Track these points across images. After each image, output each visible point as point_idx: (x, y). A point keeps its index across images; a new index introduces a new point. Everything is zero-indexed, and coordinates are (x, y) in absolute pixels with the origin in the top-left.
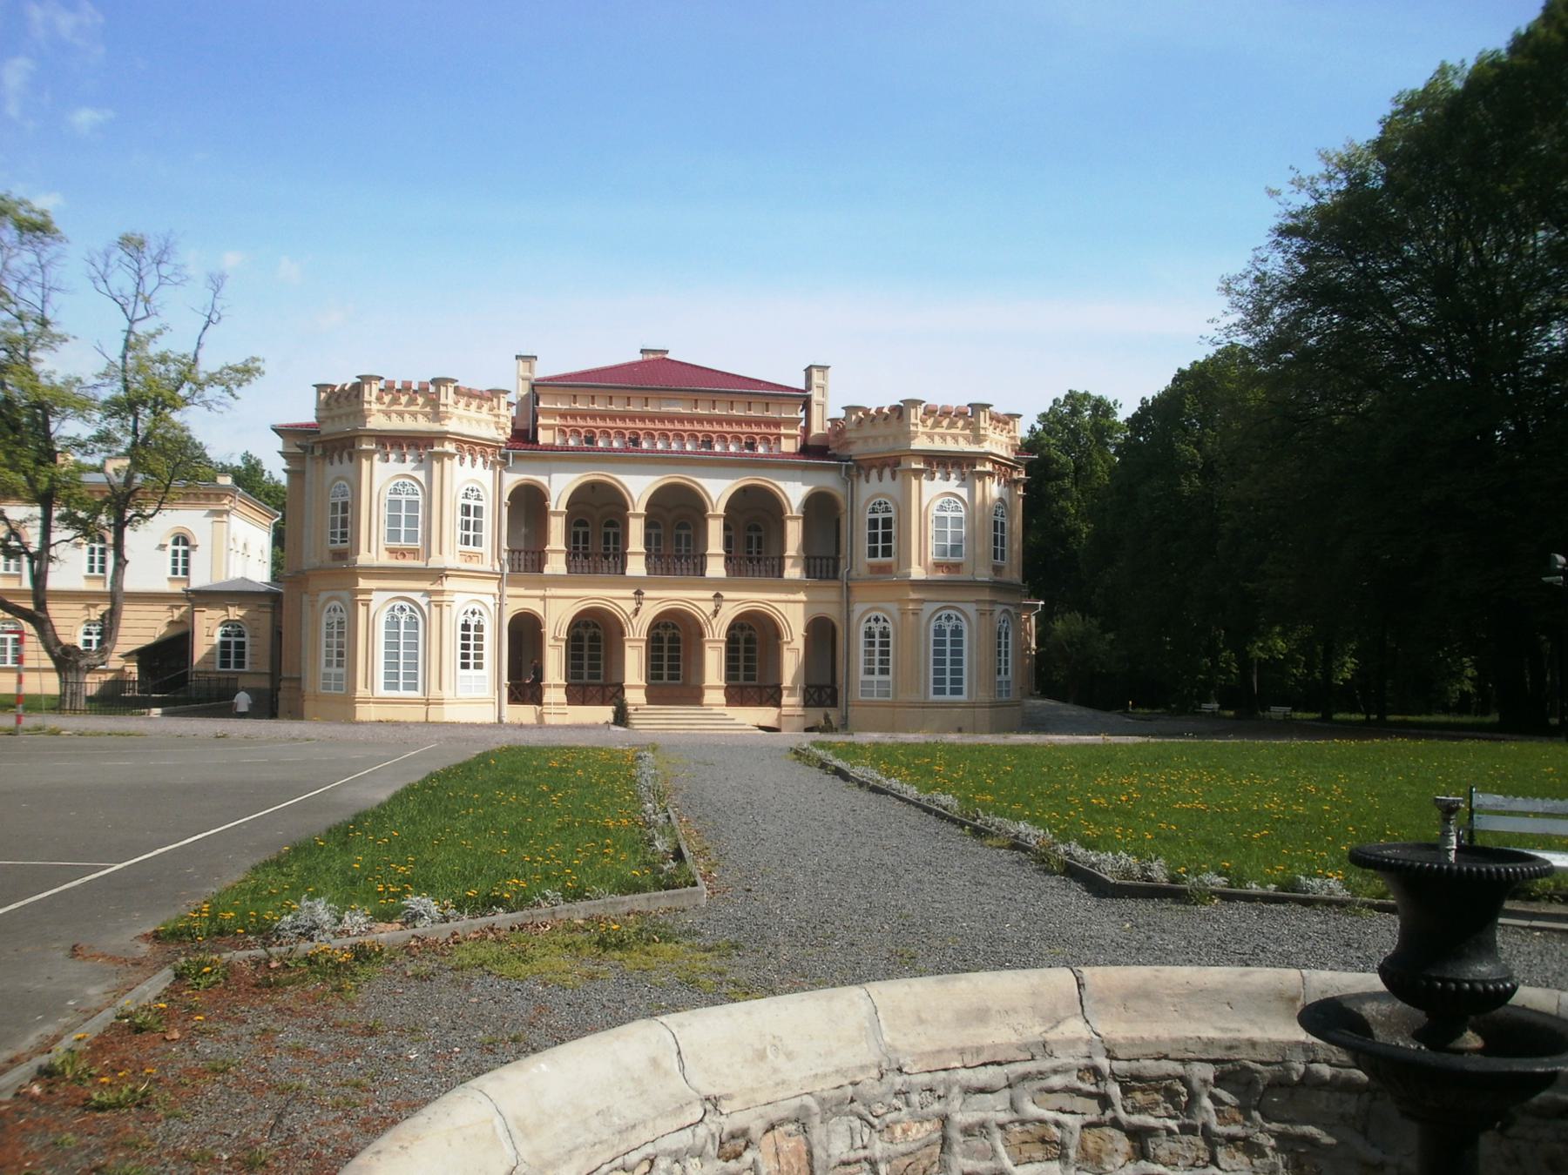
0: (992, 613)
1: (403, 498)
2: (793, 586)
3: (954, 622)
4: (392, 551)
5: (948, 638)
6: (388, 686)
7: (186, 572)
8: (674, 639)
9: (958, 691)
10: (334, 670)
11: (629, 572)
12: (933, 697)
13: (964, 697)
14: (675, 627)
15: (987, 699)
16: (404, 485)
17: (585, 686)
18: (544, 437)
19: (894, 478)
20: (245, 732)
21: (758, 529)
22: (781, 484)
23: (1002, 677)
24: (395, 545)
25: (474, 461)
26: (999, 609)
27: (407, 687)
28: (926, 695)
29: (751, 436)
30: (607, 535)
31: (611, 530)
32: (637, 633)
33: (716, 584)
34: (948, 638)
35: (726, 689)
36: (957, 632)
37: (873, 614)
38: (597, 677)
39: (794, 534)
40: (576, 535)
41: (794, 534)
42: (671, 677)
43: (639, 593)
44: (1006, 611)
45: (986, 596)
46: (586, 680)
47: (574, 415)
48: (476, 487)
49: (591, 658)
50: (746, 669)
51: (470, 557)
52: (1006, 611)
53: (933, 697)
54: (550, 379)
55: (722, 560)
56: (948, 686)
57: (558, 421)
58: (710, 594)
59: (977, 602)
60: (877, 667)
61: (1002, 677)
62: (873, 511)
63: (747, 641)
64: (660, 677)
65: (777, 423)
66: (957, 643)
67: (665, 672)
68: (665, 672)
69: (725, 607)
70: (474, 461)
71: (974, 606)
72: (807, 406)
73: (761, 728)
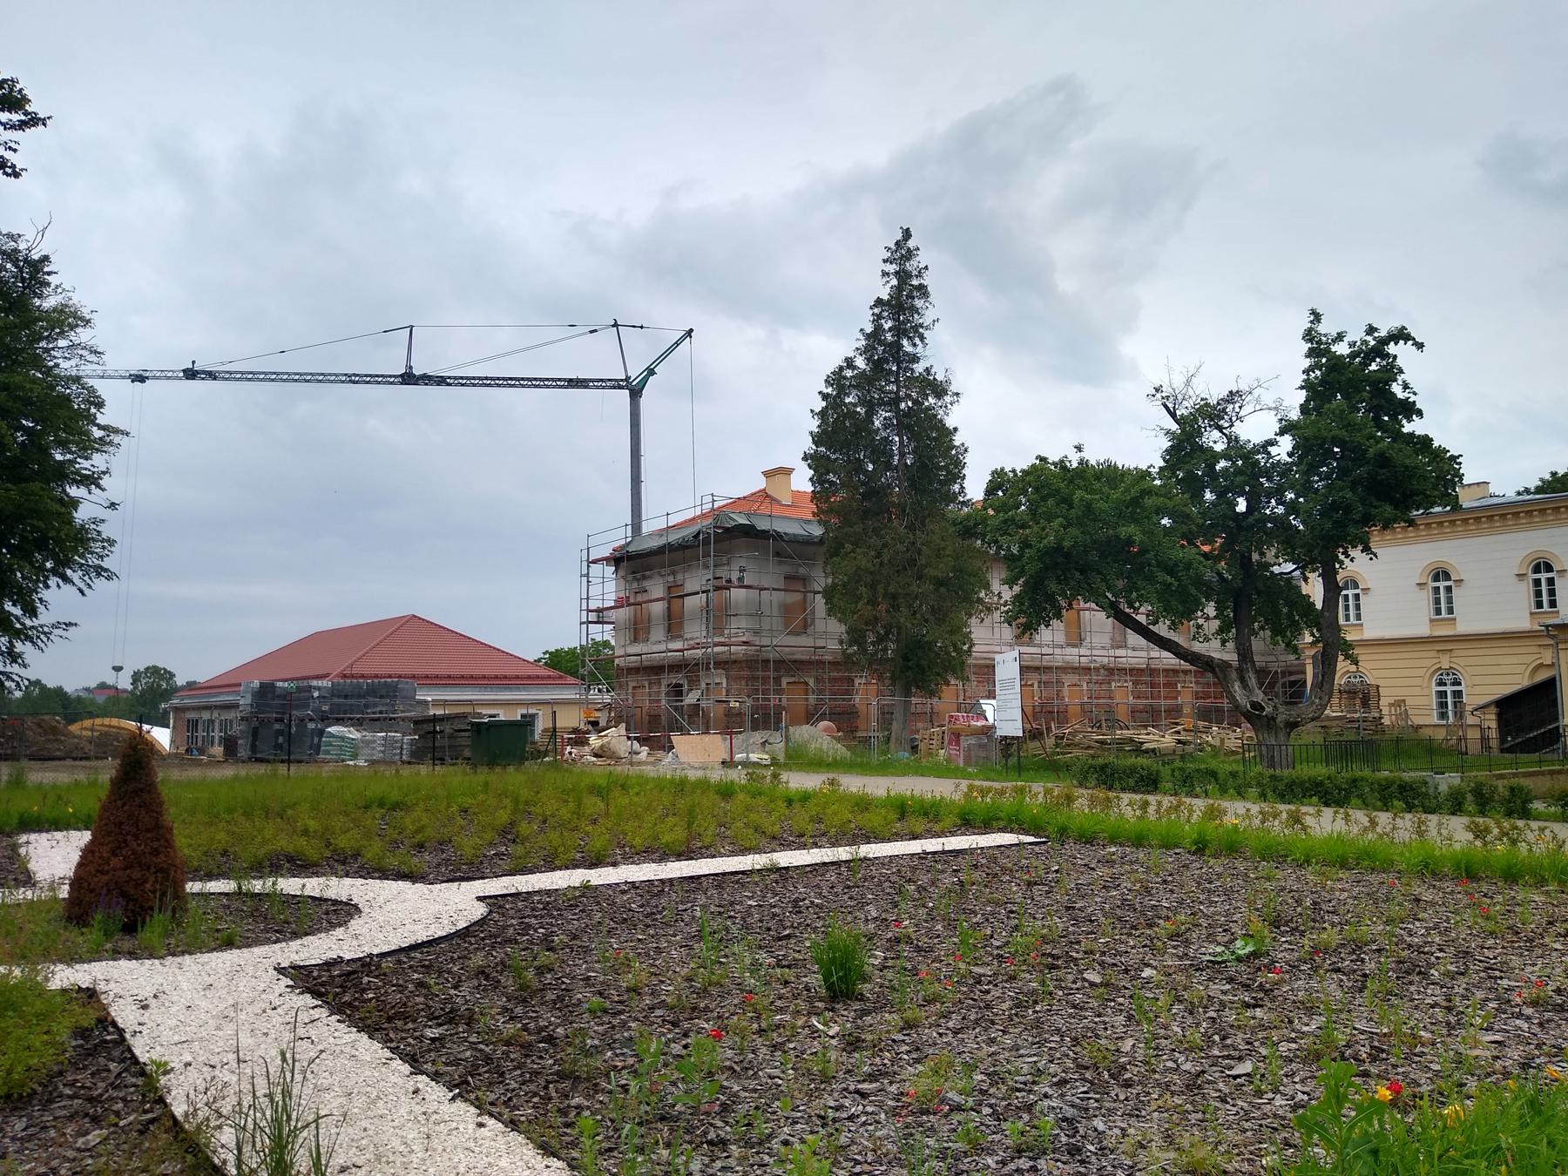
7: (1553, 604)
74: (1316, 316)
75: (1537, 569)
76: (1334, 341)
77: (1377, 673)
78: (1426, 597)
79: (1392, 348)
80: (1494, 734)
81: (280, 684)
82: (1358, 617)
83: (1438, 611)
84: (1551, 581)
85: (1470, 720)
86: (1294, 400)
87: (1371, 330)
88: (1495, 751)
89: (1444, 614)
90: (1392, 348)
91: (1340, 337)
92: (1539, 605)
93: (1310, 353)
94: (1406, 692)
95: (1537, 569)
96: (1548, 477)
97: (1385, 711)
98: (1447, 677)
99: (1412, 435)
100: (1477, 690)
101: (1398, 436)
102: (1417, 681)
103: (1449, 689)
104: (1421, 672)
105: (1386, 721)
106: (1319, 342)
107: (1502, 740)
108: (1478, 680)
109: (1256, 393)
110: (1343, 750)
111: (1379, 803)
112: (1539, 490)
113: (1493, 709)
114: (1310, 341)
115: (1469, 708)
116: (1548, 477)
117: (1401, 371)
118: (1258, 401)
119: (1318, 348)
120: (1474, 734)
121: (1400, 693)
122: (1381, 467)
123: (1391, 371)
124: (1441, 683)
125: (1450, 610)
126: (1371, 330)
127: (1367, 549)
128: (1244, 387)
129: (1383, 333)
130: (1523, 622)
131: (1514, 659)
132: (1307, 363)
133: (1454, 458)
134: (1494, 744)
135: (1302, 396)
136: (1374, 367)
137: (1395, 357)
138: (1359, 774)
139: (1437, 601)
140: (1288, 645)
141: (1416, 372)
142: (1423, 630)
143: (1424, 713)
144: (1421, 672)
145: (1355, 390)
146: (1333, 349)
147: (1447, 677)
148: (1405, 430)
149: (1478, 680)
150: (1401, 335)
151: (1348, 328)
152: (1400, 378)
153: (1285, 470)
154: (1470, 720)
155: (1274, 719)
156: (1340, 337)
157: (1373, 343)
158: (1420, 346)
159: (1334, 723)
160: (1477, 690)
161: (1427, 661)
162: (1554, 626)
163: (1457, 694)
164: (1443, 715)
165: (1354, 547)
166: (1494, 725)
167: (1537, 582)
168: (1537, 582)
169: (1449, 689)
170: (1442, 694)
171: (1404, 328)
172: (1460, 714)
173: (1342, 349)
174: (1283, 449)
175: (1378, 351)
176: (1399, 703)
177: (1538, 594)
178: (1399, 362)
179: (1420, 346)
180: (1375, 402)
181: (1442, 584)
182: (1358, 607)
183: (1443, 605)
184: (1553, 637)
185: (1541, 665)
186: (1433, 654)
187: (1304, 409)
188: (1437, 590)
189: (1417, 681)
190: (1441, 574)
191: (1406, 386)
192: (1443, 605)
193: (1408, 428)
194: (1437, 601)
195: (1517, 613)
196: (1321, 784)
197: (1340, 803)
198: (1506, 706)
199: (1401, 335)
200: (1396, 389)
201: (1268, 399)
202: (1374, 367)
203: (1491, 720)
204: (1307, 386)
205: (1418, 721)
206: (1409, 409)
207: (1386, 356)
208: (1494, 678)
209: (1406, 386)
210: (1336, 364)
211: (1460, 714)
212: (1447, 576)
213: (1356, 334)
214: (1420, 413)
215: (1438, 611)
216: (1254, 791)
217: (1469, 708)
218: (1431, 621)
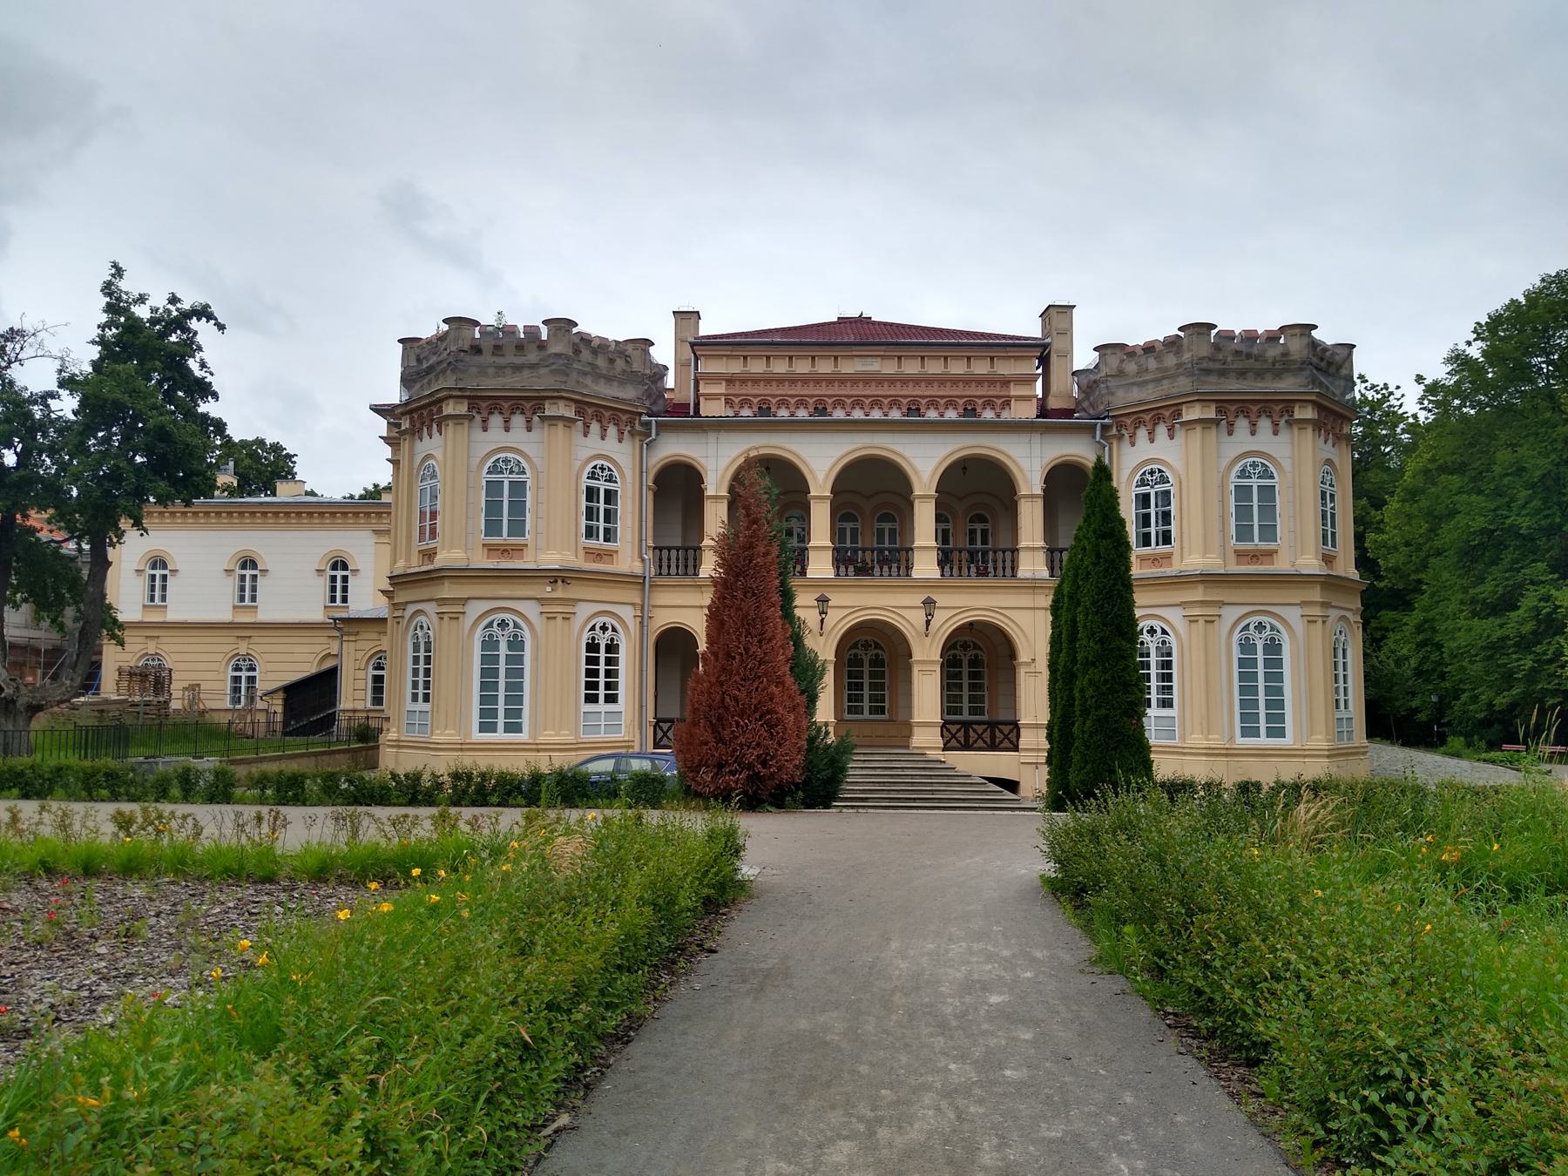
0: (1325, 618)
1: (1255, 482)
2: (1033, 586)
3: (1268, 632)
4: (491, 549)
5: (1260, 656)
6: (484, 728)
7: (345, 599)
8: (877, 662)
9: (517, 728)
10: (421, 706)
11: (915, 574)
12: (1242, 742)
13: (523, 737)
14: (877, 646)
15: (1324, 745)
16: (506, 461)
17: (966, 725)
18: (708, 409)
19: (1172, 437)
20: (1443, 776)
21: (982, 519)
22: (950, 449)
23: (1342, 713)
24: (495, 540)
25: (604, 430)
26: (1334, 614)
27: (1271, 733)
28: (1232, 738)
29: (970, 400)
30: (972, 532)
31: (979, 527)
32: (927, 654)
33: (926, 584)
34: (1260, 656)
35: (945, 726)
36: (1273, 647)
37: (600, 621)
38: (980, 711)
39: (1031, 519)
40: (842, 531)
41: (1031, 519)
42: (873, 711)
43: (823, 600)
44: (1343, 618)
45: (1316, 594)
46: (966, 716)
47: (744, 380)
48: (606, 464)
49: (873, 686)
50: (972, 699)
51: (599, 555)
52: (1343, 618)
53: (479, 737)
54: (722, 336)
55: (829, 555)
56: (501, 720)
57: (721, 389)
58: (917, 599)
59: (1303, 604)
60: (602, 692)
61: (1342, 713)
62: (1143, 483)
63: (973, 663)
64: (958, 711)
65: (1006, 382)
66: (1274, 663)
67: (866, 704)
68: (866, 704)
69: (939, 617)
70: (604, 430)
71: (1297, 611)
72: (1044, 361)
73: (991, 780)
74: (118, 271)
75: (334, 567)
76: (135, 302)
77: (175, 657)
78: (231, 584)
79: (194, 324)
80: (279, 718)
81: (594, 767)
82: (164, 598)
83: (242, 599)
84: (345, 579)
85: (260, 705)
86: (84, 357)
87: (174, 300)
88: (279, 735)
89: (247, 602)
90: (194, 324)
91: (142, 299)
92: (333, 599)
93: (109, 308)
94: (201, 678)
95: (334, 567)
96: (371, 488)
97: (176, 694)
98: (244, 664)
99: (205, 416)
100: (271, 676)
101: (190, 414)
102: (214, 666)
103: (244, 674)
104: (219, 657)
105: (175, 705)
106: (119, 299)
107: (286, 723)
108: (270, 667)
109: (41, 335)
110: (113, 732)
111: (84, 794)
112: (361, 497)
113: (281, 695)
114: (110, 295)
115: (259, 693)
116: (371, 488)
117: (200, 349)
118: (41, 345)
119: (116, 306)
120: (262, 717)
121: (194, 677)
122: (161, 440)
123: (190, 346)
124: (237, 668)
125: (253, 599)
126: (174, 300)
127: (138, 524)
128: (28, 326)
129: (186, 306)
130: (318, 616)
131: (306, 649)
132: (104, 318)
133: (289, 457)
134: (279, 727)
135: (95, 352)
136: (173, 338)
137: (196, 333)
138: (63, 762)
139: (242, 589)
140: (53, 621)
141: (217, 354)
142: (226, 616)
143: (218, 699)
144: (219, 657)
145: (148, 357)
146: (133, 309)
147: (244, 664)
148: (200, 410)
149: (270, 667)
150: (203, 312)
151: (152, 291)
152: (198, 356)
153: (64, 427)
154: (260, 705)
155: (13, 702)
156: (142, 299)
157: (175, 313)
158: (221, 327)
159: (113, 707)
160: (271, 676)
161: (226, 646)
162: (342, 620)
163: (251, 680)
164: (236, 700)
165: (42, 508)
166: (279, 709)
167: (333, 579)
168: (333, 579)
169: (244, 674)
170: (237, 679)
171: (208, 306)
172: (251, 699)
173: (142, 312)
174: (66, 406)
175: (180, 322)
176: (194, 688)
177: (333, 589)
178: (198, 338)
179: (221, 327)
180: (168, 374)
181: (248, 573)
182: (164, 588)
183: (247, 592)
184: (339, 629)
185: (329, 655)
186: (233, 640)
187: (94, 364)
188: (243, 578)
189: (214, 666)
190: (249, 563)
191: (203, 365)
192: (247, 592)
193: (203, 408)
194: (242, 589)
195: (314, 609)
196: (21, 774)
197: (40, 795)
198: (293, 692)
199: (203, 312)
200: (193, 364)
201: (54, 347)
202: (173, 338)
203: (277, 706)
204: (102, 342)
205: (210, 705)
206: (204, 390)
207: (186, 330)
208: (288, 664)
209: (203, 365)
210: (134, 325)
211: (251, 699)
212: (254, 565)
213: (159, 300)
214: (215, 396)
215: (242, 599)
216: (175, 791)
217: (259, 693)
218: (235, 607)
